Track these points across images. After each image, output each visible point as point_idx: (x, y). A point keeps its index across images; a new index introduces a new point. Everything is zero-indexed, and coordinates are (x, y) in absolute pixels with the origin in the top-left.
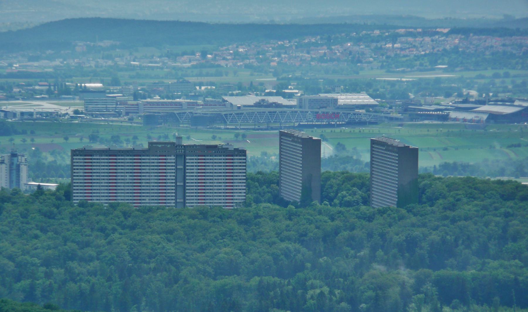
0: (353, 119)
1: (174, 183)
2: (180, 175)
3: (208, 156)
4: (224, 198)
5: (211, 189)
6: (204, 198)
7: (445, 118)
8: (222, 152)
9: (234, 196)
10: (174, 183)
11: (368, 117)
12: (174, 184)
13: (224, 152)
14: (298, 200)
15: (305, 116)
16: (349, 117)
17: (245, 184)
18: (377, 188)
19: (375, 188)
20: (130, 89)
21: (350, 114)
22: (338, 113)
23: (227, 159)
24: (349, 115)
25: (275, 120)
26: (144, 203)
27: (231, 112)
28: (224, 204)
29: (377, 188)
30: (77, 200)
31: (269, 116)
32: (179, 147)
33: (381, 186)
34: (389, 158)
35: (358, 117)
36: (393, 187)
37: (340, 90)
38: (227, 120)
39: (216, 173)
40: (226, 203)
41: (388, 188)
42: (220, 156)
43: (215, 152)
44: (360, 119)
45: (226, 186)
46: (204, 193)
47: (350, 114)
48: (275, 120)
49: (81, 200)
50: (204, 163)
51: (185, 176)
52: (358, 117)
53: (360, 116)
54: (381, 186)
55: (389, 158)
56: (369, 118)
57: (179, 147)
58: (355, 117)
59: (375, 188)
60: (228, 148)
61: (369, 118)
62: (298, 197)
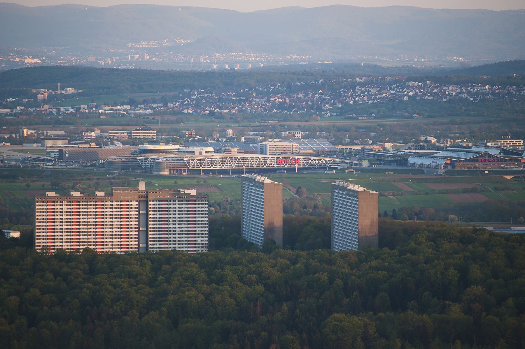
0: (314, 164)
1: (137, 245)
2: (142, 219)
3: (171, 201)
4: (186, 232)
5: (173, 244)
6: (167, 229)
7: (405, 163)
8: (184, 197)
9: (197, 241)
10: (137, 245)
11: (329, 163)
12: (137, 230)
13: (187, 197)
14: (260, 244)
15: (266, 161)
16: (309, 162)
17: (207, 219)
18: (338, 219)
19: (336, 239)
20: (92, 135)
21: (310, 159)
22: (298, 158)
23: (189, 204)
24: (309, 160)
25: (237, 165)
26: (107, 248)
27: (193, 158)
28: (186, 249)
29: (338, 232)
30: (40, 246)
31: (230, 161)
32: (142, 192)
33: (342, 207)
34: (349, 219)
35: (318, 162)
36: (354, 237)
37: (301, 136)
38: (189, 166)
39: (178, 218)
40: (189, 237)
41: (349, 226)
42: (183, 201)
43: (178, 197)
44: (320, 164)
45: (189, 224)
46: (167, 234)
47: (310, 159)
48: (237, 165)
49: (43, 246)
50: (167, 234)
51: (147, 238)
52: (318, 162)
53: (320, 161)
54: (342, 207)
55: (349, 219)
56: (329, 164)
57: (142, 192)
58: (315, 162)
59: (336, 239)
60: (191, 193)
61: (329, 164)
62: (260, 241)
